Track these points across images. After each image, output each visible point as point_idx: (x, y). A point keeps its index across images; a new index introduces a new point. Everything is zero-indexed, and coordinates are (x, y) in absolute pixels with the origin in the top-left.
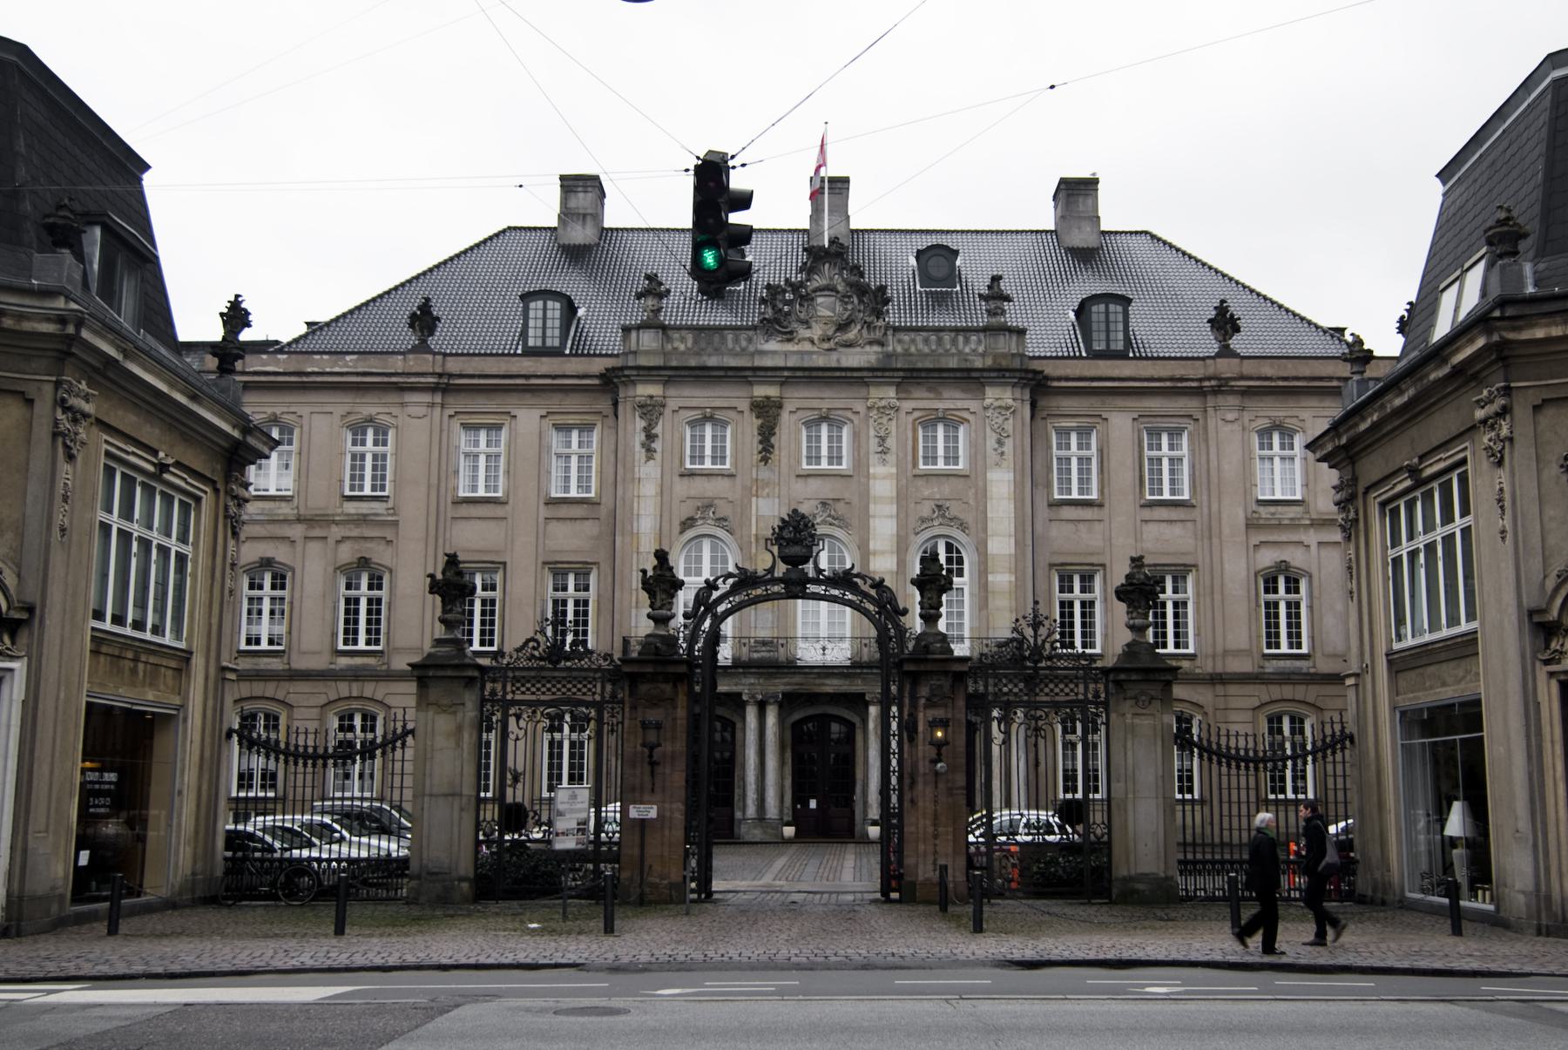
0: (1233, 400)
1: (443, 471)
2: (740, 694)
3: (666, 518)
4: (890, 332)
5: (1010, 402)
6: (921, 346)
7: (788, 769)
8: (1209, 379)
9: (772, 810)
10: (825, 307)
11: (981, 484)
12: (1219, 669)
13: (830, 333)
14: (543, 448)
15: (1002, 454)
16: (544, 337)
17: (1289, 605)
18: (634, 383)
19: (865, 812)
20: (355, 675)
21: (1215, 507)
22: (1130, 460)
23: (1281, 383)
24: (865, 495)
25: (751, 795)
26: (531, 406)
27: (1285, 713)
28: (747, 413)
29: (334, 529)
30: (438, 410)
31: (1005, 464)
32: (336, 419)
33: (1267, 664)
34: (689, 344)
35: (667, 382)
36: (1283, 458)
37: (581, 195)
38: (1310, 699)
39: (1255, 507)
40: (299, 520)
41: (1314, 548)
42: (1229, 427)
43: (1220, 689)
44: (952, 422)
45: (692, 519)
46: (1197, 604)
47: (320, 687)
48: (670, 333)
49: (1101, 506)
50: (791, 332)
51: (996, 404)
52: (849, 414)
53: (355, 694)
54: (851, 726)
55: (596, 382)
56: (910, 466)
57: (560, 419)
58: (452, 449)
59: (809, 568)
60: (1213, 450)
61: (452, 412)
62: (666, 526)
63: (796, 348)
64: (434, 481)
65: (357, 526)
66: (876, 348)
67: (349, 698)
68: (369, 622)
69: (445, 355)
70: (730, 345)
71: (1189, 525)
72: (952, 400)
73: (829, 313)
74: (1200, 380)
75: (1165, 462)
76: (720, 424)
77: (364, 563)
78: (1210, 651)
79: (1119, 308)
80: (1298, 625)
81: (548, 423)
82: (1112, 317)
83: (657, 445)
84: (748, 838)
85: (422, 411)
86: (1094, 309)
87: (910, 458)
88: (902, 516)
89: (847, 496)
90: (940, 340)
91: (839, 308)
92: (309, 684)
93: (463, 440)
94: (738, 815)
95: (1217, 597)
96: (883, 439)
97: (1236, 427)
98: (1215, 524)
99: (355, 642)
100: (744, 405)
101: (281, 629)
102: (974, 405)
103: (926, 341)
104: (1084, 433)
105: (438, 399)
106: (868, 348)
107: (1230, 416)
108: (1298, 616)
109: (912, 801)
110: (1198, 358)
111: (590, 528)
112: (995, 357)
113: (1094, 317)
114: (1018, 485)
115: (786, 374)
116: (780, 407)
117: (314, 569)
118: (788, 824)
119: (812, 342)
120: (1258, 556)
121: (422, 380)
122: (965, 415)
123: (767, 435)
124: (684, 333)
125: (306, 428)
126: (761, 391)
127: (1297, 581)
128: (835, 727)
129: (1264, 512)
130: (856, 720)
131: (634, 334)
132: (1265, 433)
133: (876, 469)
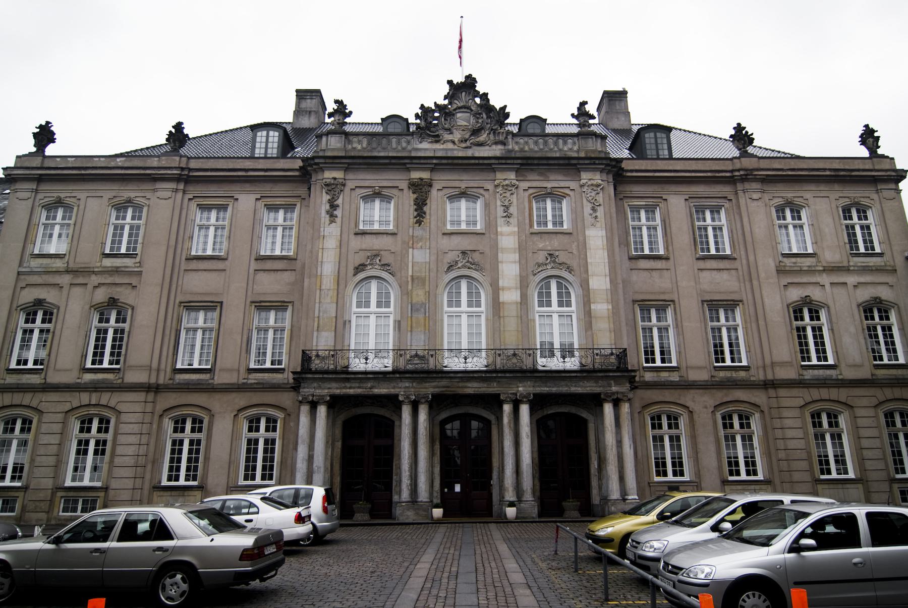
0: (755, 185)
1: (181, 234)
2: (397, 396)
3: (343, 264)
4: (510, 137)
5: (600, 182)
6: (532, 146)
7: (437, 459)
8: (739, 170)
9: (423, 494)
10: (463, 119)
11: (581, 238)
12: (770, 377)
13: (467, 136)
14: (256, 221)
15: (596, 217)
16: (266, 148)
17: (813, 329)
18: (322, 170)
19: (502, 496)
20: (95, 387)
21: (751, 258)
22: (686, 226)
23: (790, 173)
24: (495, 247)
25: (406, 481)
26: (249, 192)
27: (823, 410)
28: (406, 190)
29: (93, 277)
30: (180, 195)
31: (598, 225)
32: (105, 200)
33: (805, 372)
34: (364, 145)
35: (347, 169)
36: (795, 227)
37: (309, 101)
38: (843, 400)
39: (781, 258)
40: (68, 271)
41: (828, 286)
42: (755, 203)
43: (772, 392)
44: (556, 196)
45: (364, 265)
46: (745, 329)
47: (67, 396)
48: (351, 138)
49: (667, 259)
50: (438, 136)
51: (589, 183)
52: (481, 191)
53: (93, 402)
54: (487, 423)
55: (297, 173)
56: (527, 227)
57: (270, 201)
58: (189, 222)
60: (745, 220)
61: (191, 196)
62: (343, 270)
63: (442, 147)
64: (172, 243)
65: (111, 275)
66: (500, 147)
67: (89, 405)
68: (113, 347)
69: (189, 158)
70: (394, 145)
71: (733, 272)
72: (555, 181)
73: (466, 124)
74: (732, 171)
75: (710, 230)
76: (387, 199)
77: (113, 302)
78: (760, 363)
79: (664, 135)
80: (823, 344)
81: (261, 204)
82: (659, 141)
83: (338, 212)
84: (402, 519)
85: (169, 194)
86: (647, 135)
87: (527, 221)
88: (523, 262)
89: (480, 248)
90: (546, 143)
91: (472, 120)
92: (59, 394)
93: (199, 217)
94: (395, 498)
95: (761, 322)
96: (506, 208)
97: (759, 203)
98: (753, 271)
99: (101, 362)
100: (404, 185)
101: (43, 354)
102: (573, 185)
103: (536, 143)
104: (650, 210)
105: (181, 186)
106: (494, 147)
107: (755, 196)
108: (822, 337)
110: (727, 159)
111: (288, 277)
112: (587, 152)
113: (647, 141)
114: (610, 239)
115: (435, 161)
116: (431, 186)
117: (74, 307)
118: (437, 506)
119: (454, 142)
120: (788, 293)
121: (169, 172)
122: (567, 191)
123: (420, 205)
124: (361, 138)
125: (82, 207)
126: (416, 175)
127: (817, 312)
128: (475, 424)
129: (788, 262)
130: (492, 418)
131: (324, 139)
132: (780, 210)
133: (503, 228)
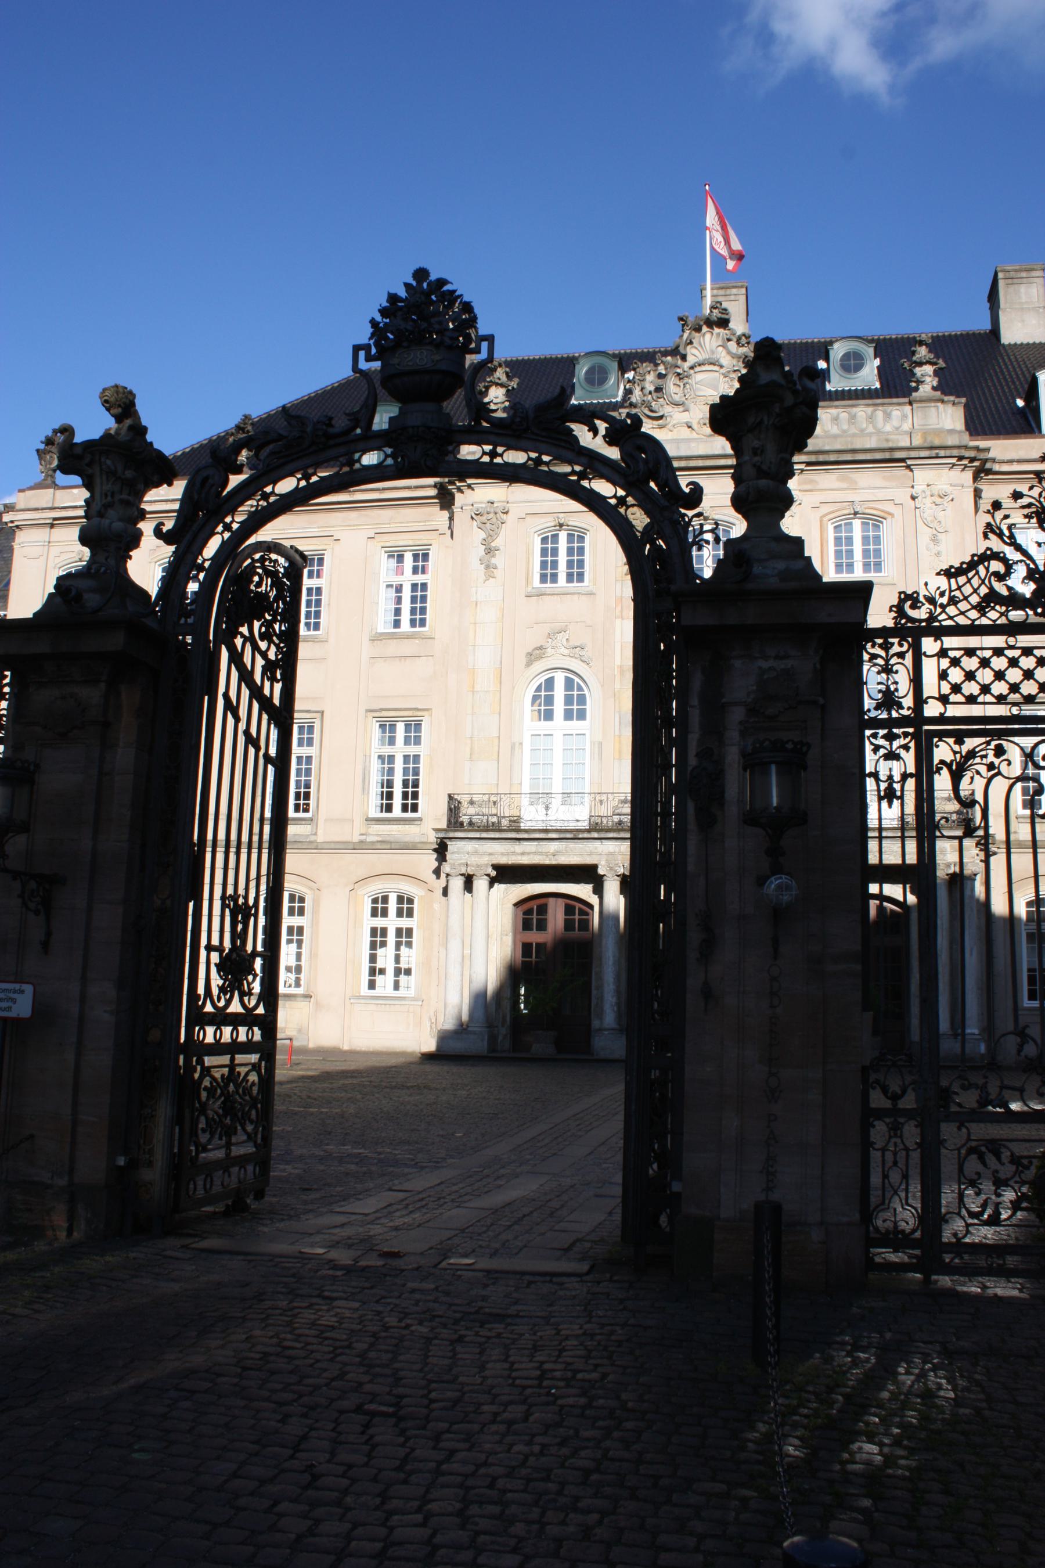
5: (947, 488)
50: (661, 417)
59: (455, 406)
94: (596, 1024)
109: (707, 993)
122: (888, 507)
